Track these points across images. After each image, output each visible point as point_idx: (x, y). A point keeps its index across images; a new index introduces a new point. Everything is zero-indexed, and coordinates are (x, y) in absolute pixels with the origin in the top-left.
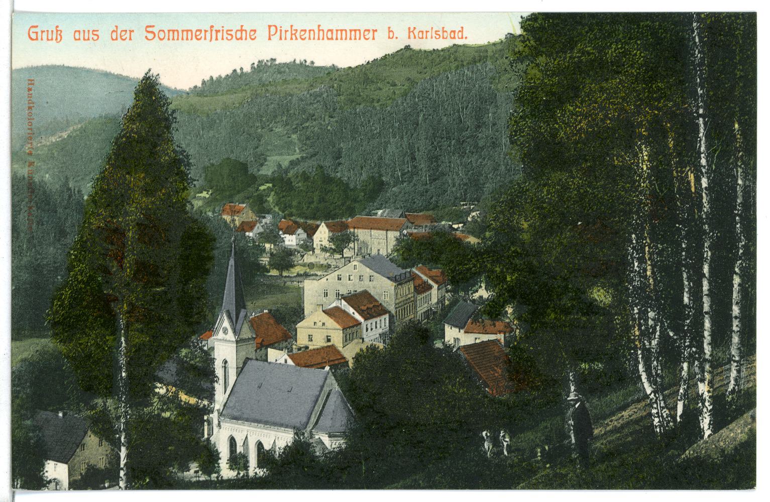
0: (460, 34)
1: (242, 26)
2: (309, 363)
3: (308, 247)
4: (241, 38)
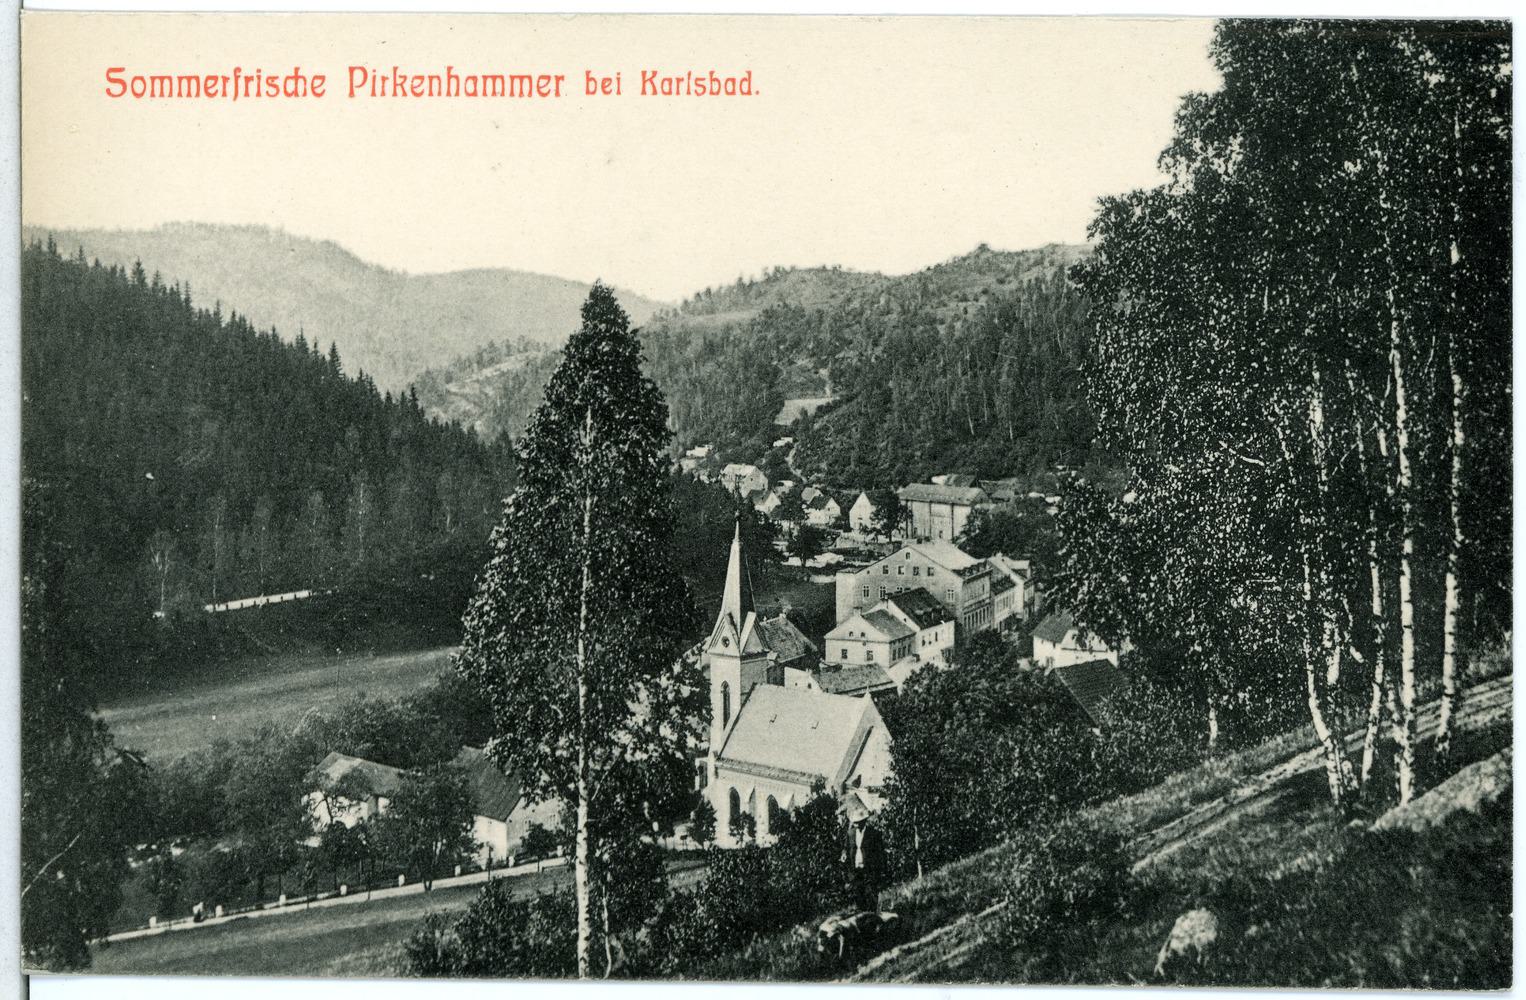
0: (745, 84)
1: (297, 69)
2: (842, 688)
3: (843, 523)
4: (295, 93)
